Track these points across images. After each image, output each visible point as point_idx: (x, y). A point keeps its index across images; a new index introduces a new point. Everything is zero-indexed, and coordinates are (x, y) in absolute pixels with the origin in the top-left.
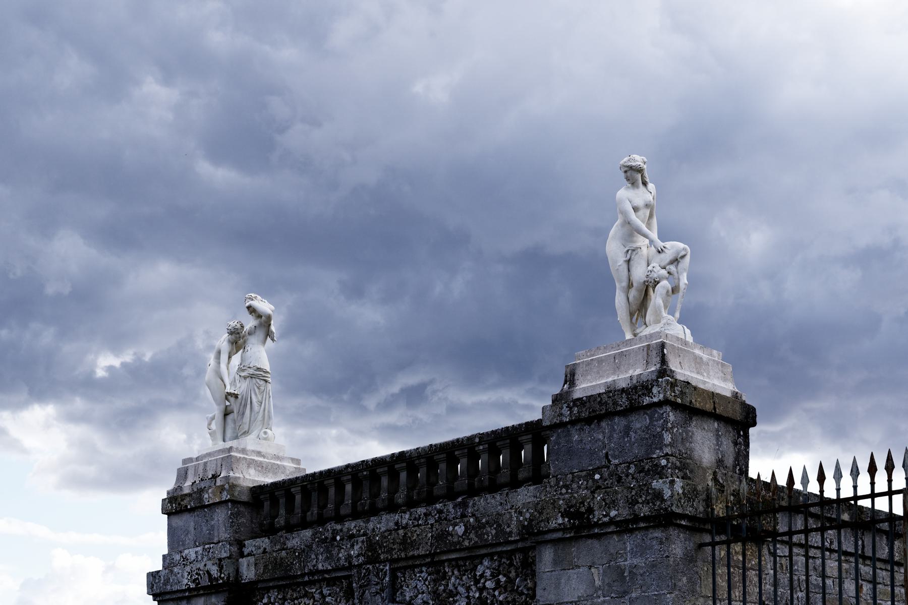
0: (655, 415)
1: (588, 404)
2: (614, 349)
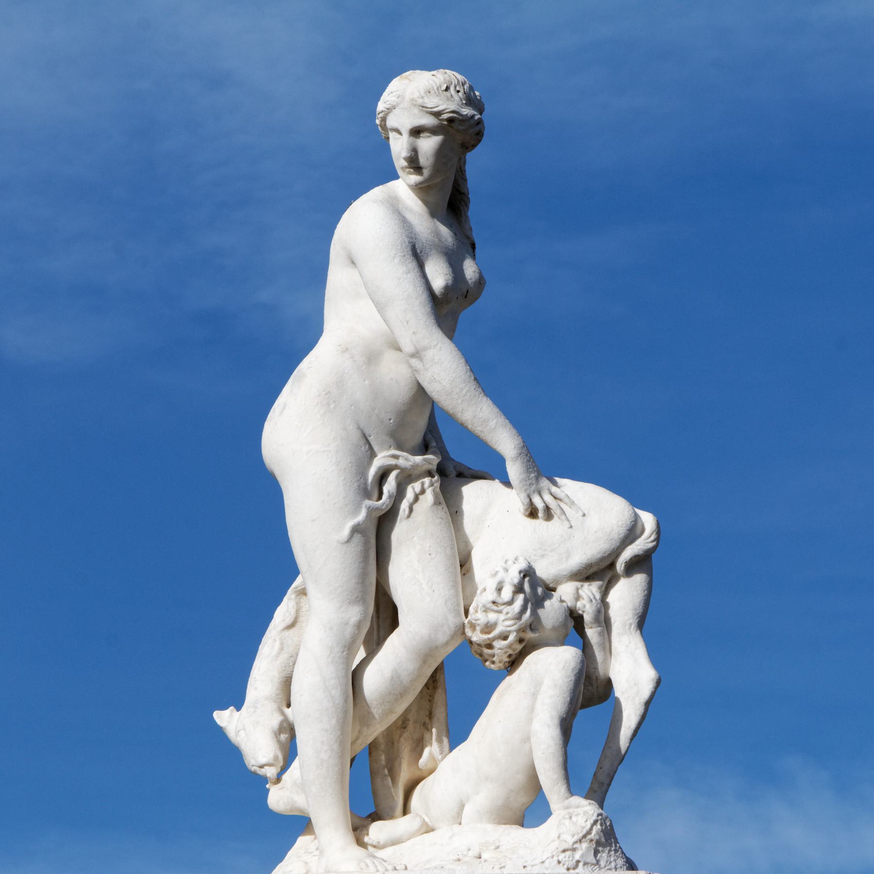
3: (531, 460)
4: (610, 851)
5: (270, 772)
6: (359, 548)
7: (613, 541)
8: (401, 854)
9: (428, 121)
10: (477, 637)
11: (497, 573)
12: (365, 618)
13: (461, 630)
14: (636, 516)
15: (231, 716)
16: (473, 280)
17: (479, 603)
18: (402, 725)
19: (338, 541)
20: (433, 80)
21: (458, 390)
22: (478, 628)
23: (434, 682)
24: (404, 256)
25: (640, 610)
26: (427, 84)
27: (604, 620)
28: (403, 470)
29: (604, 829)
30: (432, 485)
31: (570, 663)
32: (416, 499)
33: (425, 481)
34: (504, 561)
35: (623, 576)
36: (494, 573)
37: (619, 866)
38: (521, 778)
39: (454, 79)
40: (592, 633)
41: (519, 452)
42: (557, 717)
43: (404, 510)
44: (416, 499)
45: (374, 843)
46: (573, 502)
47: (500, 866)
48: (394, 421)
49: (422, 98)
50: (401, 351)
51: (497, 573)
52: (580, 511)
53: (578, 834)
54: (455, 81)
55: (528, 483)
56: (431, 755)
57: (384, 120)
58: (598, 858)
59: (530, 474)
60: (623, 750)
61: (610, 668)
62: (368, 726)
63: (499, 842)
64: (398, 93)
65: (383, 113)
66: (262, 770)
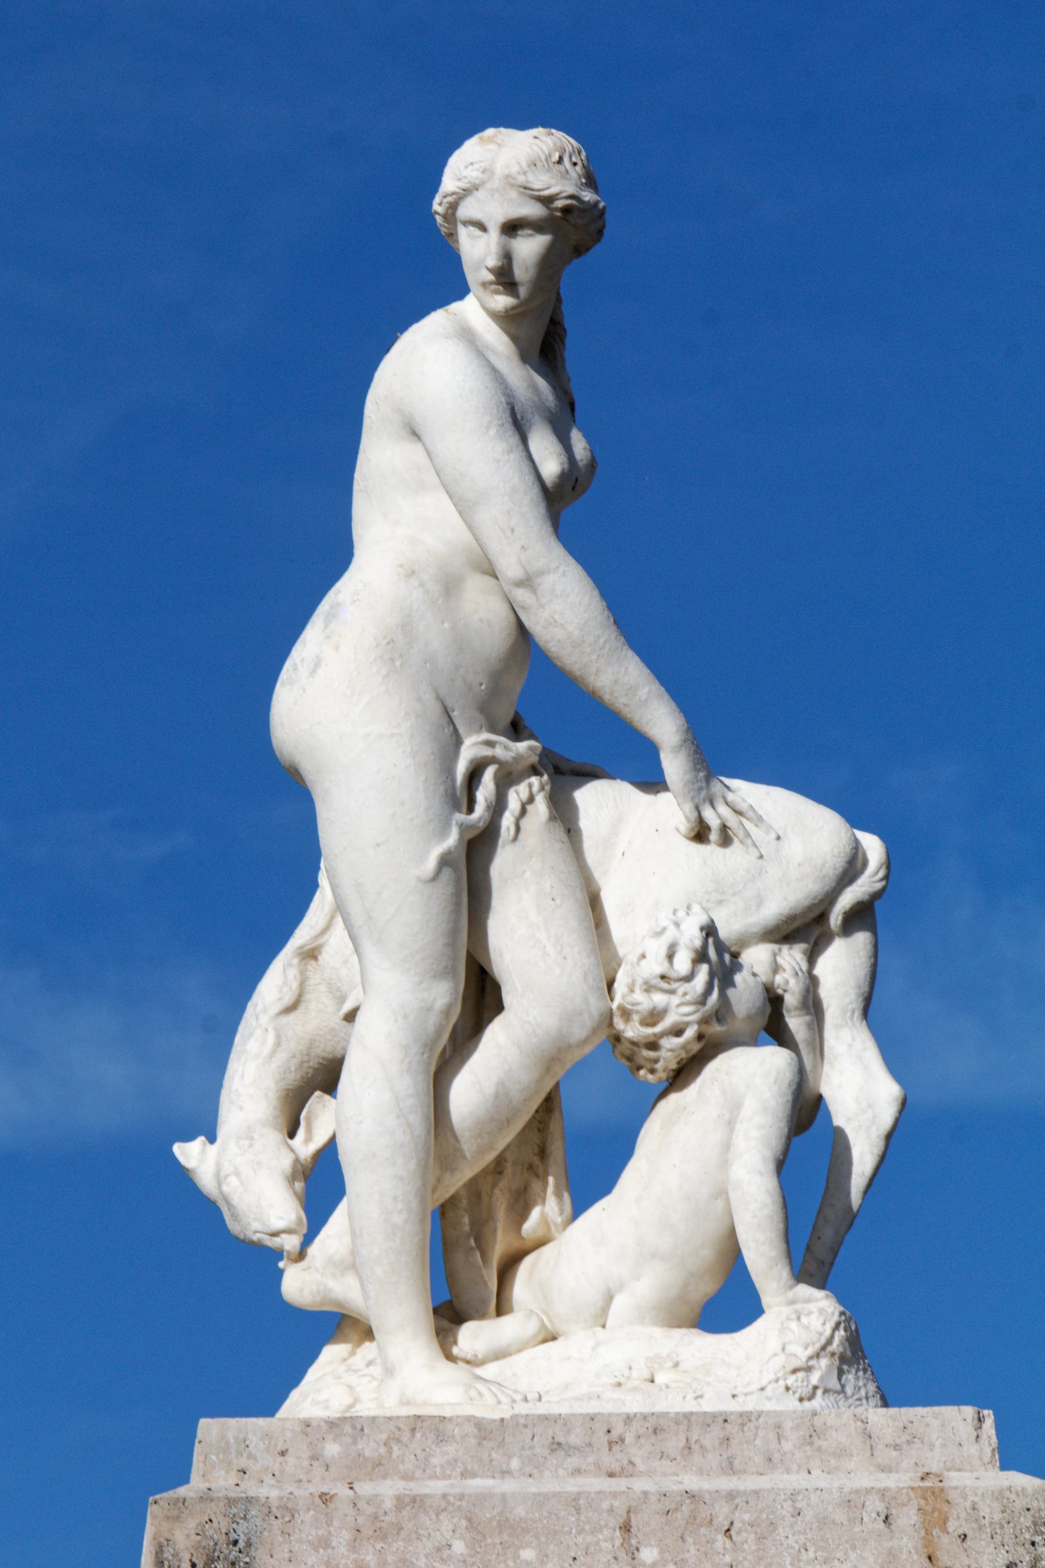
2: (573, 1462)
3: (699, 751)
4: (858, 1370)
5: (290, 1243)
6: (450, 890)
7: (827, 878)
8: (514, 1375)
9: (532, 210)
10: (632, 1031)
12: (456, 999)
13: (608, 1018)
15: (203, 1151)
16: (585, 462)
17: (637, 978)
18: (495, 1168)
19: (419, 879)
20: (538, 146)
21: (592, 639)
22: (636, 1018)
24: (503, 425)
25: (866, 989)
26: (530, 151)
27: (812, 1005)
29: (848, 1336)
30: (542, 788)
31: (784, 1074)
32: (523, 812)
33: (533, 783)
34: (672, 911)
35: (838, 935)
36: (659, 929)
37: (870, 1394)
38: (708, 1254)
39: (567, 144)
40: (796, 1023)
41: (683, 738)
42: (772, 1160)
43: (508, 829)
44: (523, 812)
45: (469, 1357)
46: (761, 817)
47: (695, 1395)
48: (486, 688)
49: (525, 173)
50: (497, 578)
51: (664, 930)
52: (773, 832)
53: (813, 1344)
54: (569, 149)
55: (696, 786)
56: (544, 1219)
57: (454, 207)
58: (843, 1382)
59: (698, 772)
61: (821, 1080)
62: (453, 1171)
63: (678, 1355)
64: (483, 165)
65: (454, 196)
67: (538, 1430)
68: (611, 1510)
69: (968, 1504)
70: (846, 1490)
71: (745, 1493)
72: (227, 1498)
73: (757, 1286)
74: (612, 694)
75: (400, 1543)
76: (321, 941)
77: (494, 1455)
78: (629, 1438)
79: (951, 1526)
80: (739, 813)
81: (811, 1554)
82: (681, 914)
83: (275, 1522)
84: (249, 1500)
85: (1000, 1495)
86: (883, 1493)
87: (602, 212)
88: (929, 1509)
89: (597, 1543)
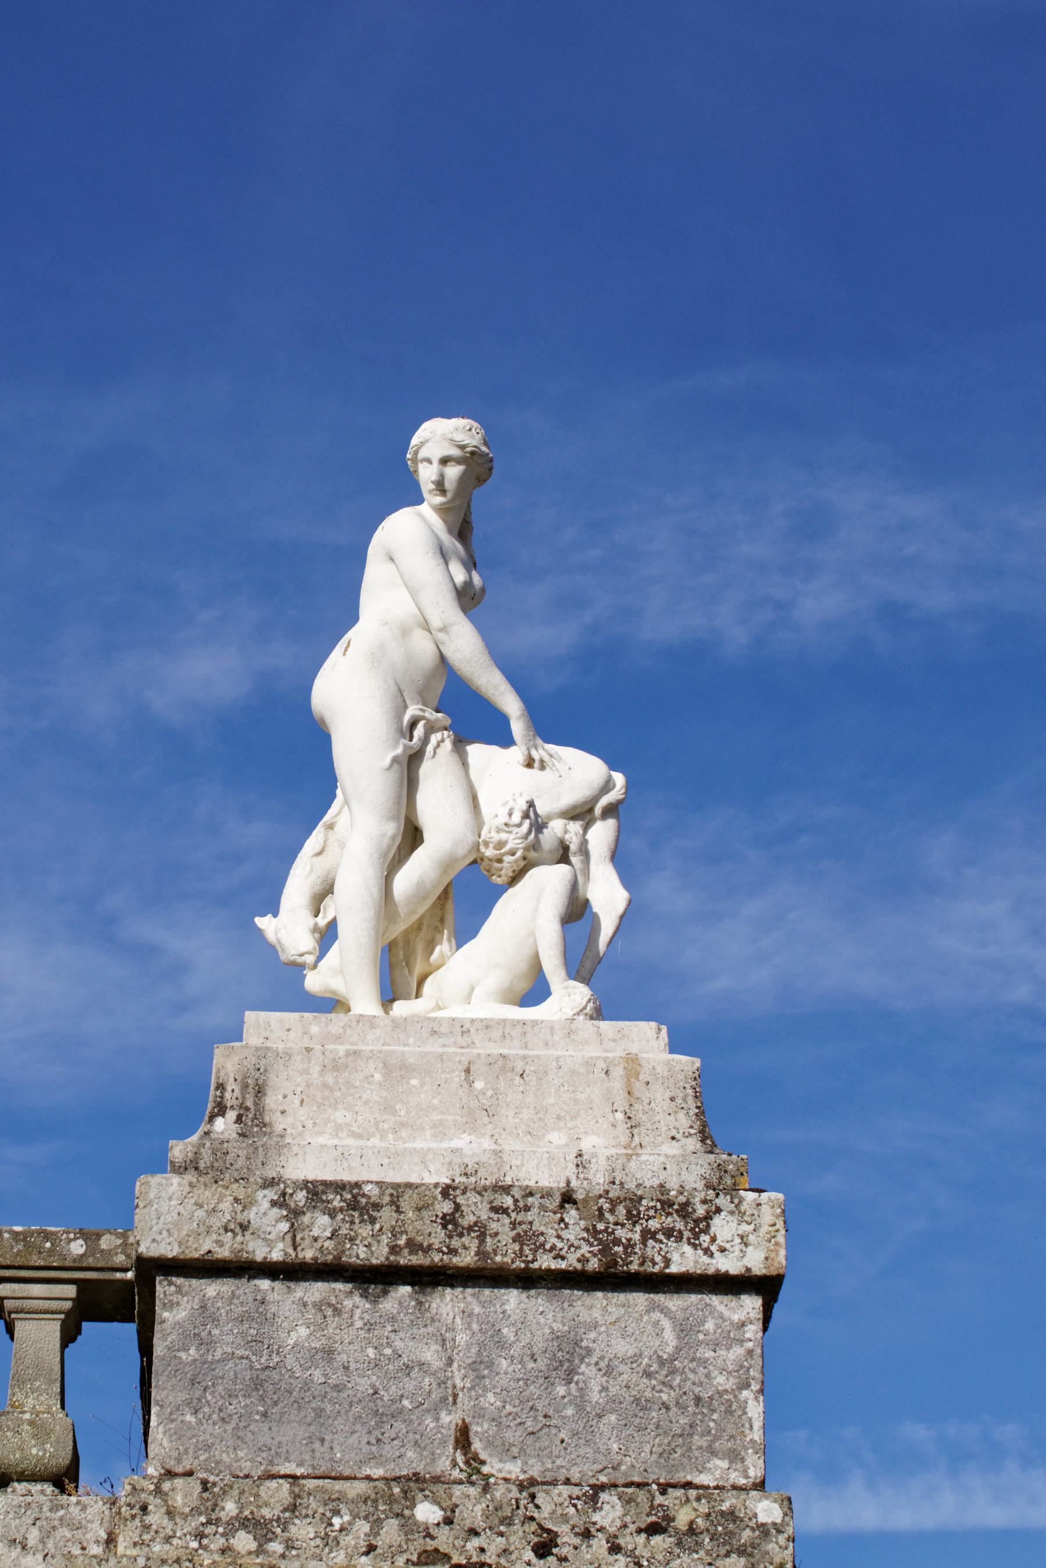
0: (703, 1322)
1: (387, 1216)
2: (443, 1040)
5: (310, 959)
9: (455, 452)
10: (489, 852)
11: (507, 803)
13: (476, 847)
14: (610, 776)
22: (491, 845)
23: (446, 893)
25: (613, 847)
27: (584, 851)
28: (428, 721)
30: (449, 737)
32: (438, 745)
44: (438, 745)
51: (507, 803)
56: (441, 952)
57: (416, 453)
60: (601, 953)
66: (303, 958)
67: (424, 1024)
68: (460, 1062)
69: (650, 1067)
70: (586, 1057)
71: (532, 1056)
72: (256, 1047)
73: (549, 980)
74: (486, 688)
75: (347, 1073)
76: (336, 820)
77: (400, 1036)
78: (472, 1030)
79: (641, 1077)
80: (551, 756)
81: (566, 1088)
82: (517, 796)
83: (280, 1060)
84: (267, 1048)
85: (667, 1063)
86: (605, 1059)
87: (491, 460)
88: (630, 1068)
89: (452, 1078)
